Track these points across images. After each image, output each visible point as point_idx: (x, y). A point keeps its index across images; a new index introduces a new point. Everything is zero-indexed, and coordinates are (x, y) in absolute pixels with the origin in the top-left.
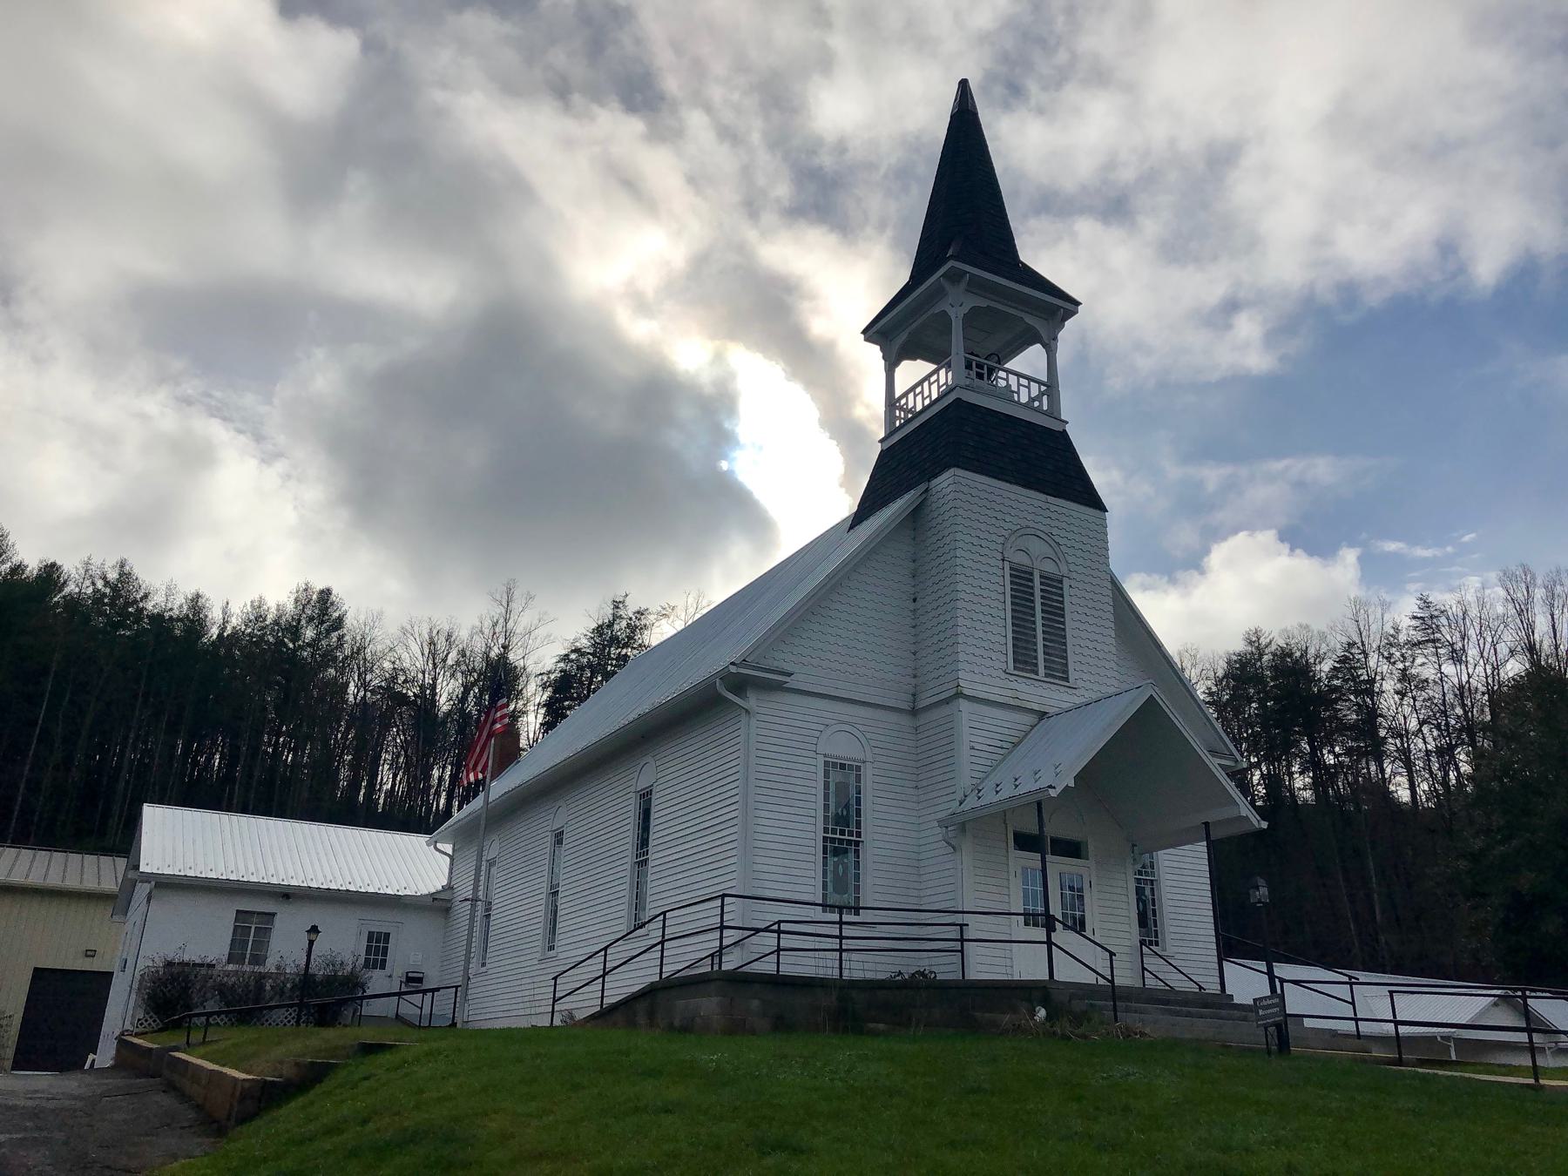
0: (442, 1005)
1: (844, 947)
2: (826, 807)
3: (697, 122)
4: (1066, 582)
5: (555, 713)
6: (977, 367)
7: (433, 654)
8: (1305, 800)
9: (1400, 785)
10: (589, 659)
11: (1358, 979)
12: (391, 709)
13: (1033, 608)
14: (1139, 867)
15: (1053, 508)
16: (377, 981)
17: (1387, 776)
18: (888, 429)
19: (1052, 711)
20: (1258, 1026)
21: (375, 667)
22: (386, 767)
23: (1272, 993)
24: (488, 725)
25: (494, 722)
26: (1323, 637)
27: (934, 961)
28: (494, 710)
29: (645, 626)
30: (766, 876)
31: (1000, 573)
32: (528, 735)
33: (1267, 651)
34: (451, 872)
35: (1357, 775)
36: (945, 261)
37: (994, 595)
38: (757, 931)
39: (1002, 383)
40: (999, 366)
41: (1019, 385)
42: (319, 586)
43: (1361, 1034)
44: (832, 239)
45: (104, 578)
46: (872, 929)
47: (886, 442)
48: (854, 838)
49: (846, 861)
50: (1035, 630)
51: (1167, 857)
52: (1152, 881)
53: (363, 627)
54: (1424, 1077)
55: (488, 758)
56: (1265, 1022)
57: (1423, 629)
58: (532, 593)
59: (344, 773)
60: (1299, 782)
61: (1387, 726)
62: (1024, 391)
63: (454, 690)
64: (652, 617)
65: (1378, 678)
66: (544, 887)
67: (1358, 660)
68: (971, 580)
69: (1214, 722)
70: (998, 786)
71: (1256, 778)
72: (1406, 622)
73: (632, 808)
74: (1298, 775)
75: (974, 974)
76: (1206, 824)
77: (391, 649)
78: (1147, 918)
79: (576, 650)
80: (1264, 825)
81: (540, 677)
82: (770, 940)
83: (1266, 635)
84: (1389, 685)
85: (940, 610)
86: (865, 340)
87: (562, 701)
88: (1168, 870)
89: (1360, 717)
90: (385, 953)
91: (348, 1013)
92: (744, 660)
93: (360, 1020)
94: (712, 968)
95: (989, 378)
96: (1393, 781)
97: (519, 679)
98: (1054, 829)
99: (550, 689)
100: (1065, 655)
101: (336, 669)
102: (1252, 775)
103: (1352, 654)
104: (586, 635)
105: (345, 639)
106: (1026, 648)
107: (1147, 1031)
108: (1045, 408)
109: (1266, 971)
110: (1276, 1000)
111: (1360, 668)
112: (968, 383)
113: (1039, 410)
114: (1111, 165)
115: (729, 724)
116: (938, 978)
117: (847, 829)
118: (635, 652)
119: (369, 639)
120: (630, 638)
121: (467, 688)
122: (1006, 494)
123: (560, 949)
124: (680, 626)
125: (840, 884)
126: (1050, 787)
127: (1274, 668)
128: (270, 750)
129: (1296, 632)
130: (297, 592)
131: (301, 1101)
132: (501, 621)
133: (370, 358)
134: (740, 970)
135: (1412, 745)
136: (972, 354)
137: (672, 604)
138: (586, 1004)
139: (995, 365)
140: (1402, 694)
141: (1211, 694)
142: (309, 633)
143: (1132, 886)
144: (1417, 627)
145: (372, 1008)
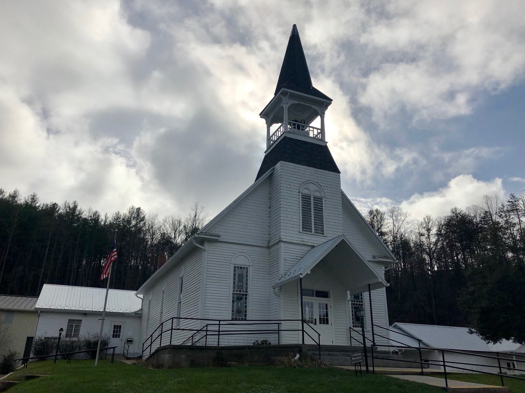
2: (234, 283)
3: (265, 44)
4: (324, 199)
13: (311, 209)
15: (318, 173)
19: (316, 245)
24: (110, 259)
25: (112, 257)
31: (298, 197)
37: (295, 205)
45: (70, 207)
48: (245, 293)
56: (355, 362)
57: (512, 206)
68: (286, 200)
73: (179, 281)
76: (369, 285)
83: (459, 210)
86: (260, 117)
100: (323, 225)
113: (318, 139)
122: (300, 169)
126: (301, 274)
130: (130, 209)
134: (182, 345)
142: (134, 223)
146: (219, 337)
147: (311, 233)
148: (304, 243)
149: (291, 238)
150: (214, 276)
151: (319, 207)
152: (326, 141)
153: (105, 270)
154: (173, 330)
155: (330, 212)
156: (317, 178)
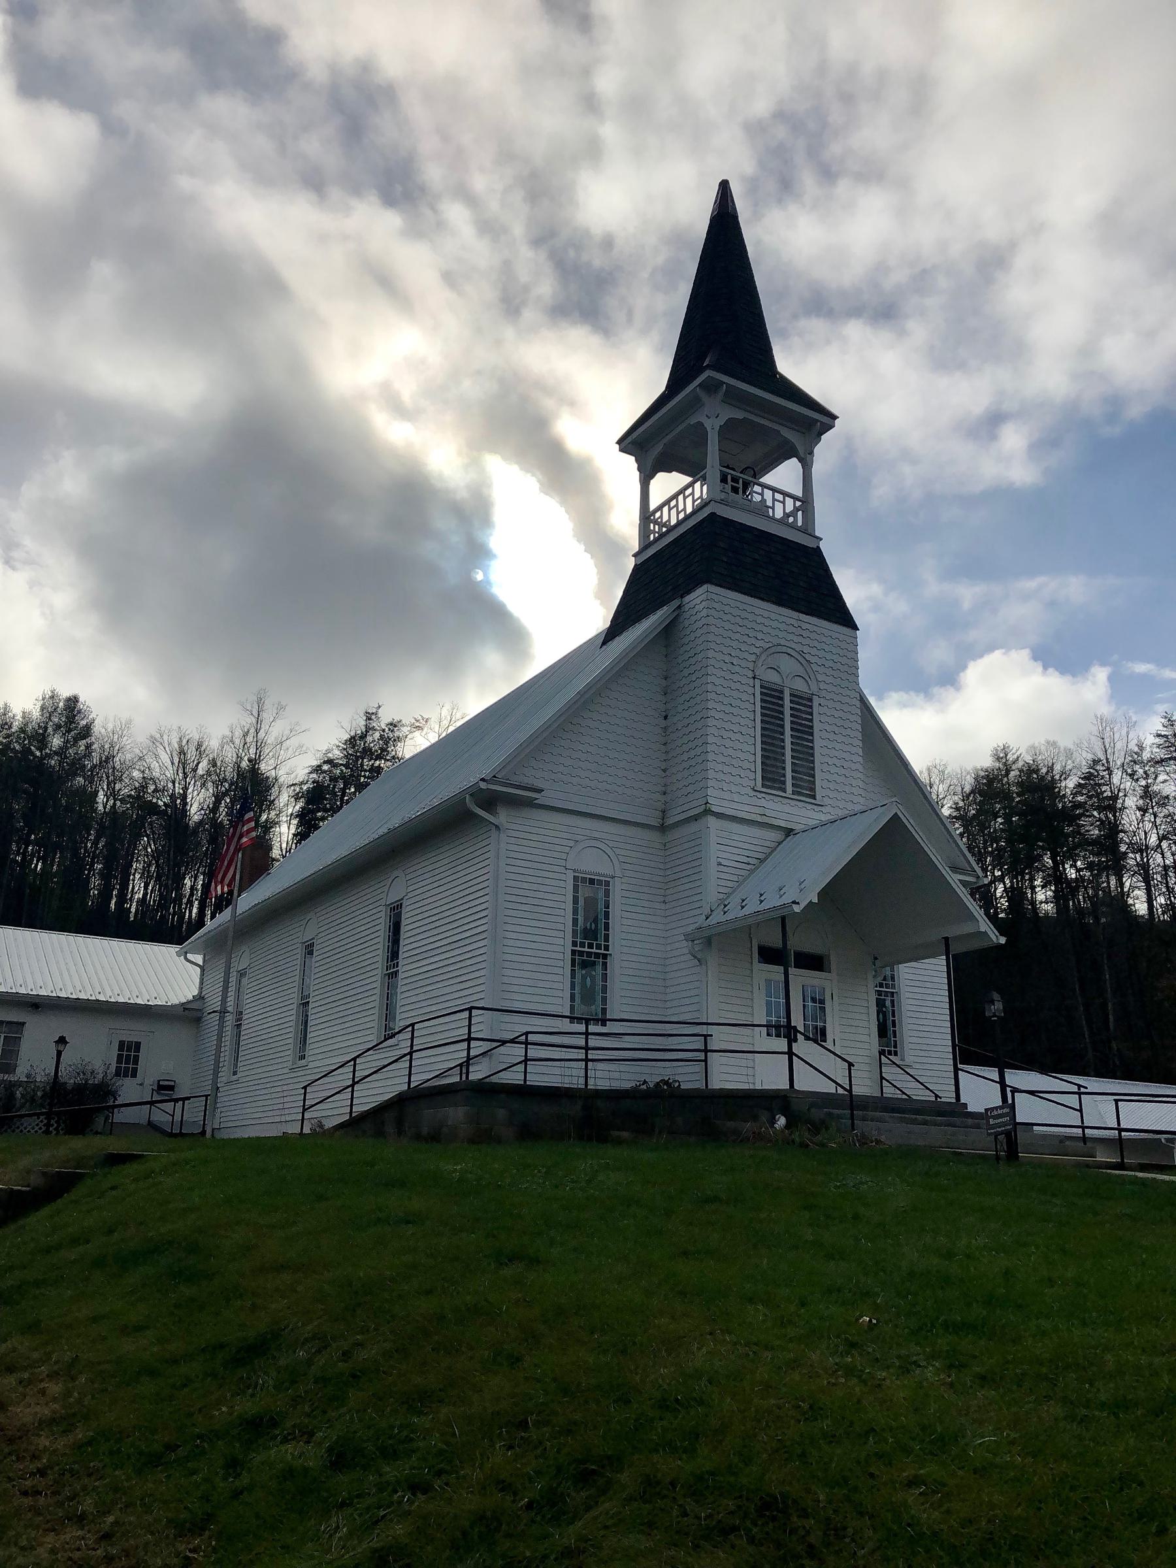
0: (193, 1113)
1: (590, 1057)
2: (575, 921)
3: (457, 214)
5: (307, 824)
6: (732, 481)
7: (183, 763)
8: (1047, 912)
9: (1137, 899)
10: (342, 770)
11: (1086, 1088)
12: (142, 819)
13: (782, 726)
14: (879, 979)
16: (129, 1090)
17: (1126, 890)
18: (642, 543)
19: (798, 828)
20: (989, 1134)
21: (125, 775)
22: (138, 876)
23: (1003, 1103)
24: (236, 839)
25: (241, 836)
26: (1069, 754)
27: (680, 1070)
28: (241, 824)
29: (398, 738)
30: (515, 988)
31: (751, 690)
32: (281, 845)
33: (1013, 768)
34: (201, 983)
35: (1096, 889)
36: (701, 370)
38: (504, 1042)
39: (757, 498)
40: (755, 480)
41: (774, 500)
42: (65, 692)
43: (1087, 1136)
44: (595, 340)
46: (620, 1039)
47: (641, 555)
49: (594, 973)
50: (783, 748)
51: (907, 970)
52: (893, 993)
53: (111, 734)
54: (1143, 1182)
55: (236, 868)
56: (995, 1130)
58: (284, 703)
59: (95, 882)
60: (1041, 896)
61: (1127, 841)
62: (779, 509)
63: (205, 800)
64: (405, 730)
65: (1121, 794)
66: (295, 1000)
67: (1103, 777)
68: (721, 698)
69: (958, 839)
70: (743, 901)
71: (999, 893)
72: (1150, 740)
74: (1040, 889)
75: (717, 1083)
76: (946, 939)
77: (140, 758)
78: (887, 1029)
79: (329, 761)
80: (1003, 940)
81: (292, 788)
82: (518, 1051)
83: (1014, 751)
84: (1132, 802)
85: (691, 728)
87: (314, 812)
88: (907, 982)
89: (1102, 833)
90: (136, 1062)
91: (100, 1121)
92: (494, 777)
93: (112, 1129)
94: (461, 1078)
95: (744, 492)
96: (1132, 896)
97: (270, 789)
98: (799, 942)
99: (303, 800)
101: (84, 778)
102: (996, 889)
103: (1096, 770)
104: (339, 746)
105: (93, 748)
106: (773, 766)
107: (883, 1138)
108: (800, 524)
109: (998, 1080)
110: (1006, 1110)
111: (1104, 785)
112: (723, 498)
113: (793, 526)
114: (881, 268)
115: (480, 838)
116: (682, 1087)
117: (595, 943)
118: (389, 763)
119: (117, 748)
120: (383, 750)
121: (218, 799)
122: (757, 611)
123: (311, 1059)
124: (433, 738)
125: (588, 996)
126: (794, 902)
127: (1020, 784)
128: (19, 858)
129: (1043, 748)
130: (43, 700)
131: (45, 1211)
132: (252, 730)
133: (117, 459)
135: (1152, 859)
136: (728, 467)
137: (426, 716)
138: (335, 1113)
139: (751, 479)
140: (1143, 810)
141: (957, 809)
142: (56, 742)
143: (873, 998)
144: (1161, 745)
145: (120, 1116)
146: (586, 1066)
147: (784, 794)
148: (765, 820)
149: (735, 806)
150: (524, 900)
151: (803, 722)
152: (817, 534)
153: (219, 873)
154: (472, 1042)
155: (832, 737)
156: (800, 639)
